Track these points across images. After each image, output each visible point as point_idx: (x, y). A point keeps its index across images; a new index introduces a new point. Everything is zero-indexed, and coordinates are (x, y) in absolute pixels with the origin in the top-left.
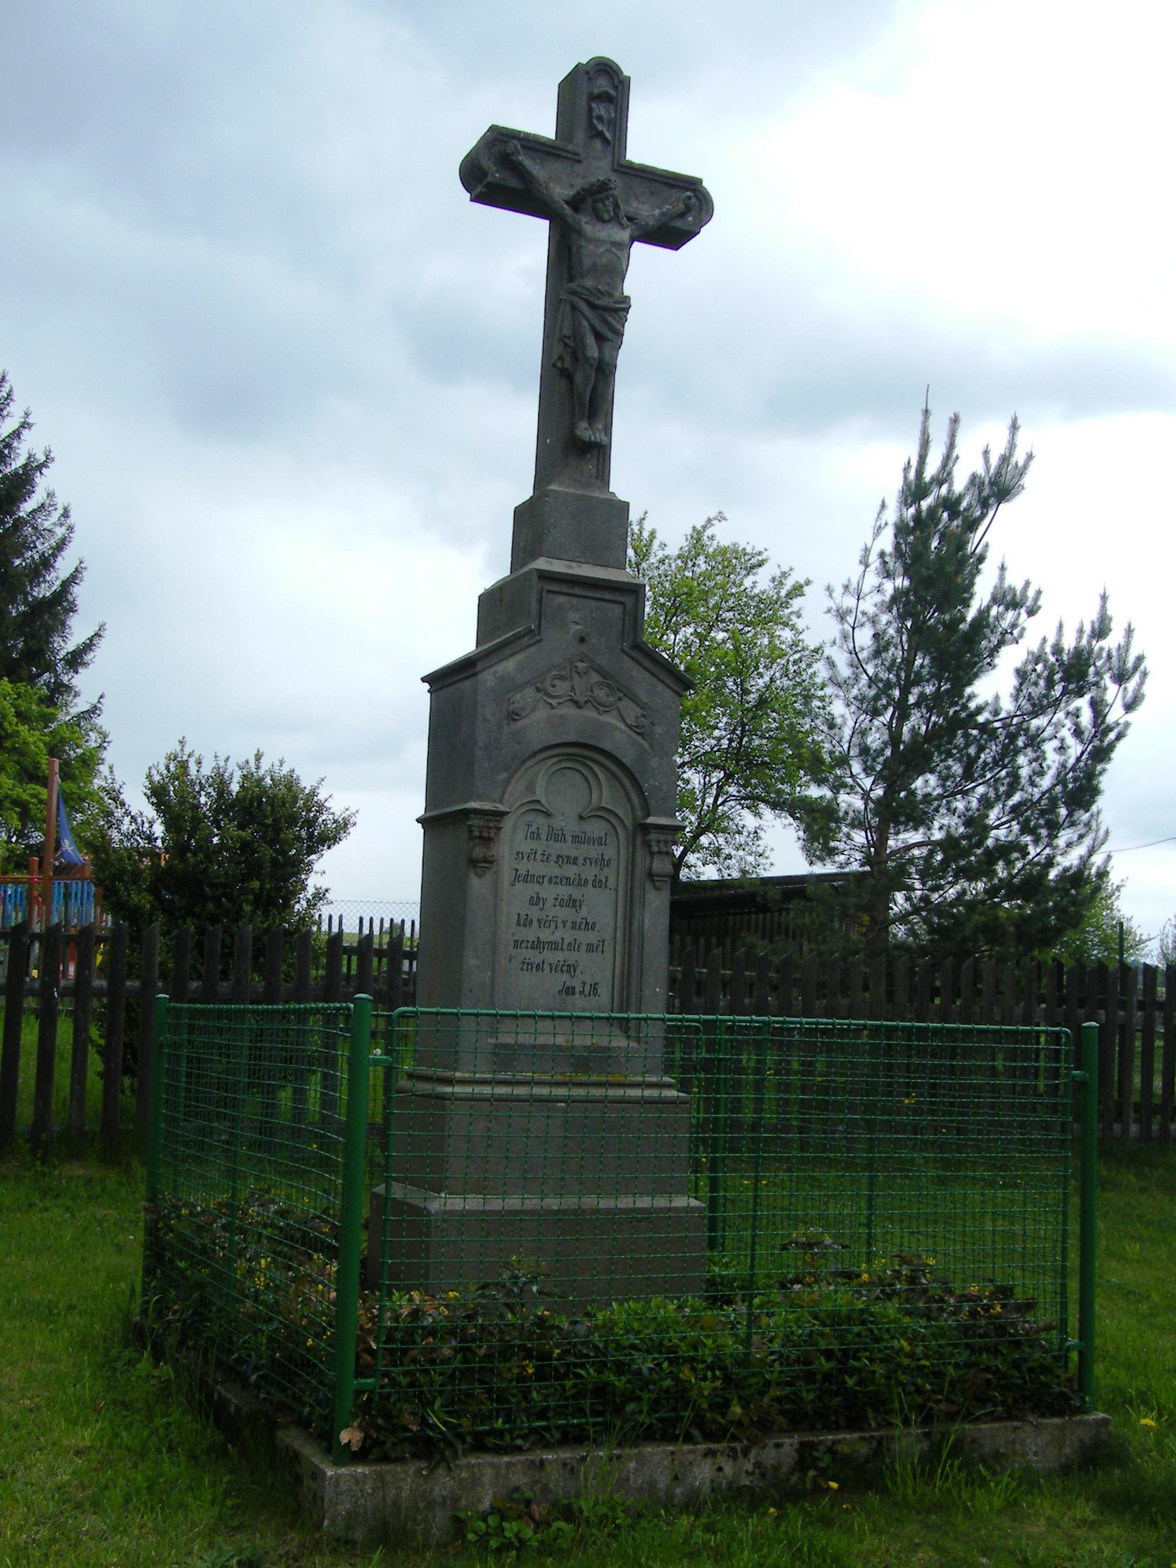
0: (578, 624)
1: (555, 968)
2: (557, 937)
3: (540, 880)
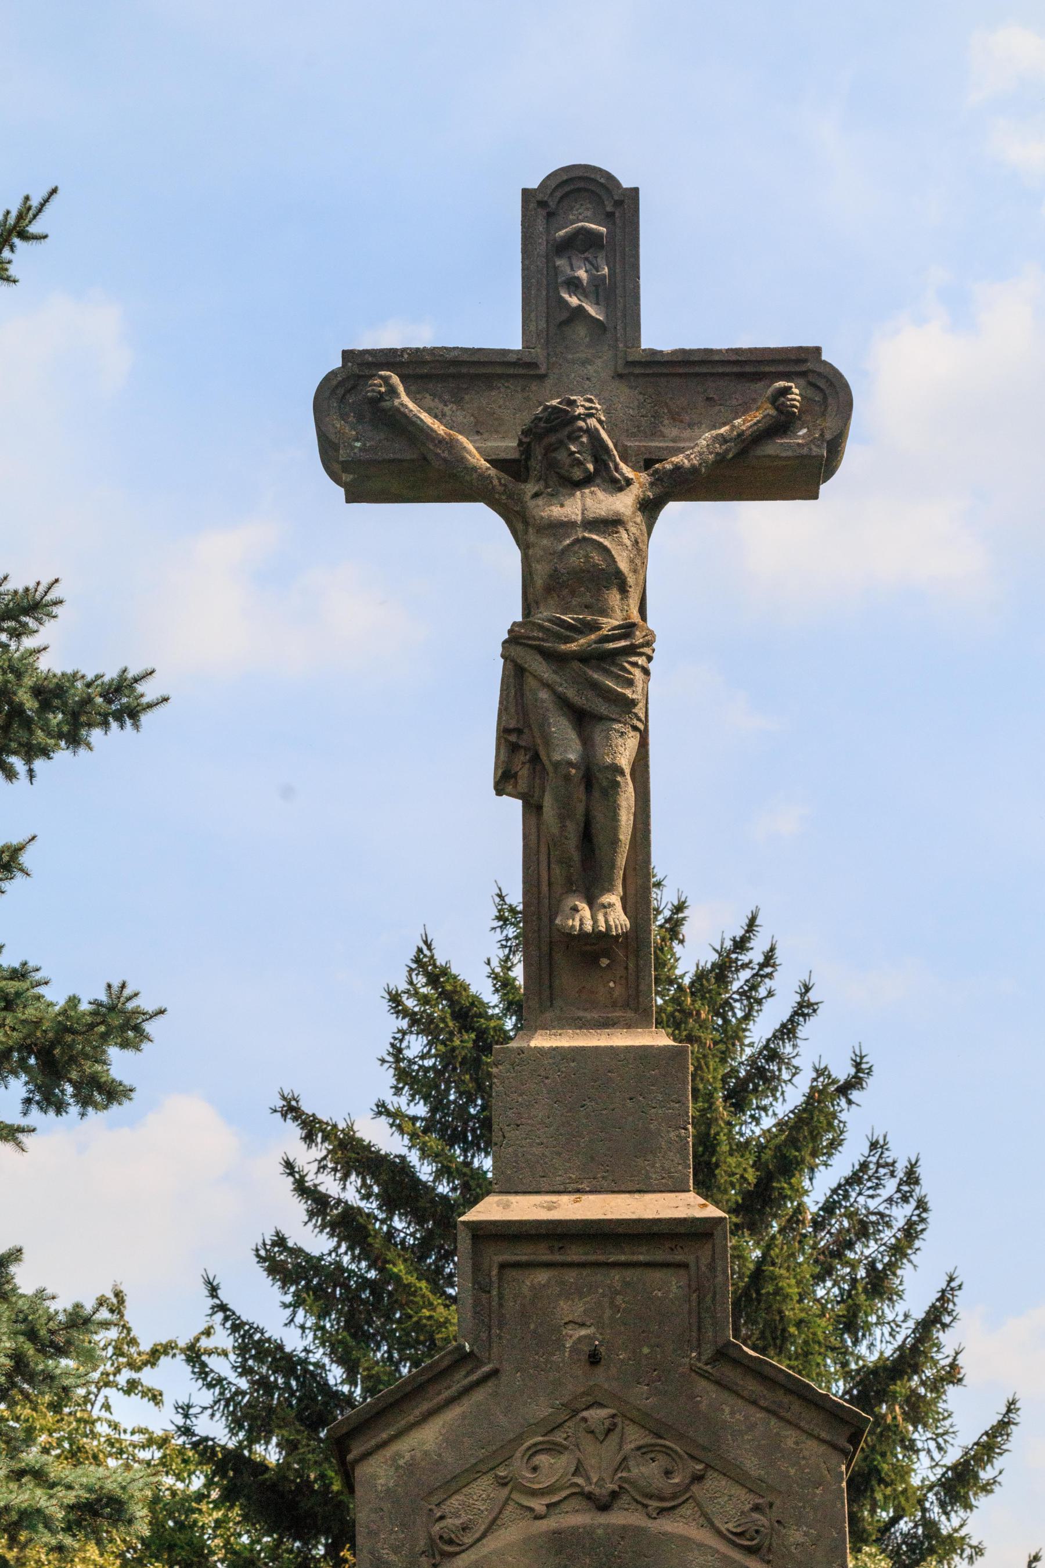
0: (583, 1325)
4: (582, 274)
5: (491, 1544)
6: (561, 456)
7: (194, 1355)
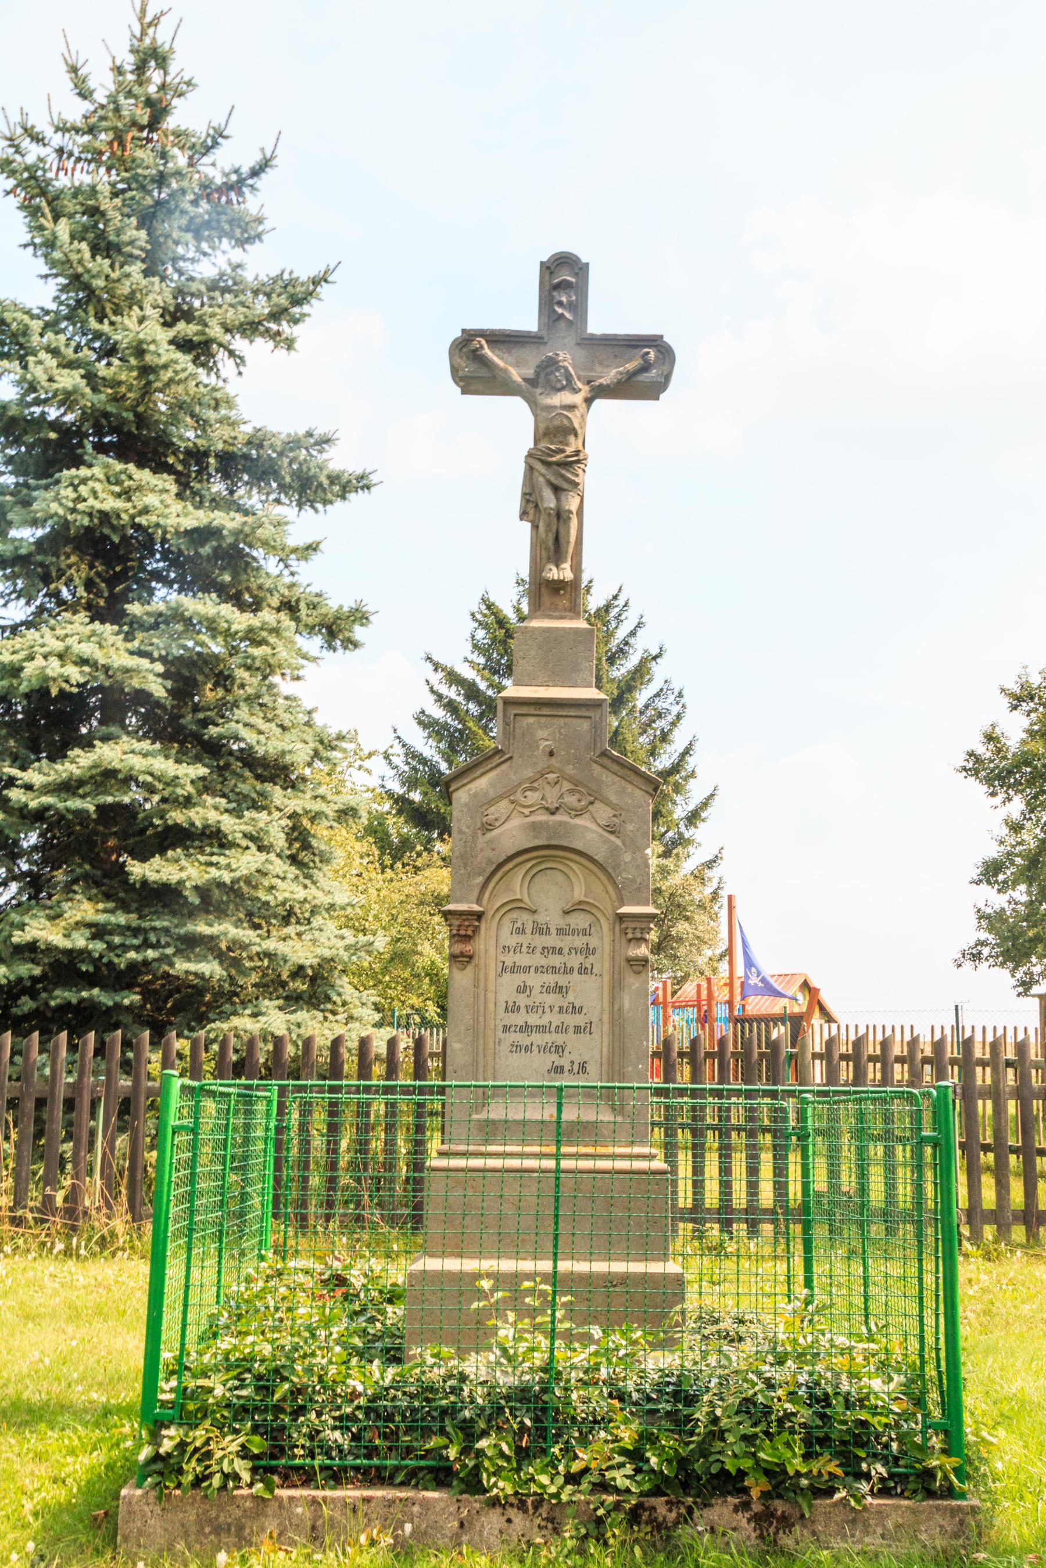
1: (544, 1049)
2: (544, 1021)
3: (527, 969)
4: (564, 299)
5: (506, 826)
6: (552, 377)
7: (387, 757)
